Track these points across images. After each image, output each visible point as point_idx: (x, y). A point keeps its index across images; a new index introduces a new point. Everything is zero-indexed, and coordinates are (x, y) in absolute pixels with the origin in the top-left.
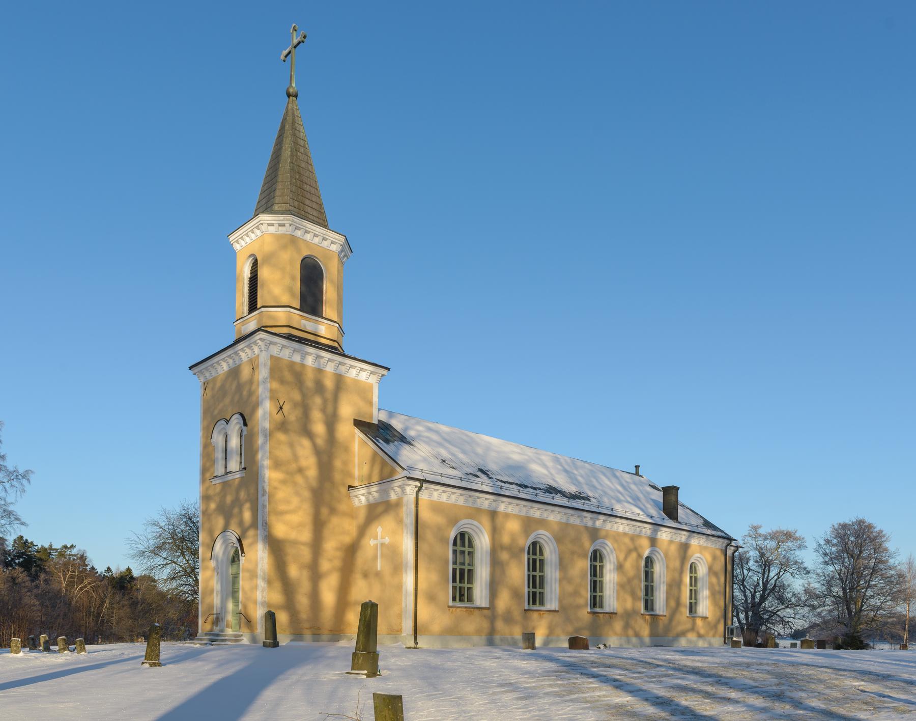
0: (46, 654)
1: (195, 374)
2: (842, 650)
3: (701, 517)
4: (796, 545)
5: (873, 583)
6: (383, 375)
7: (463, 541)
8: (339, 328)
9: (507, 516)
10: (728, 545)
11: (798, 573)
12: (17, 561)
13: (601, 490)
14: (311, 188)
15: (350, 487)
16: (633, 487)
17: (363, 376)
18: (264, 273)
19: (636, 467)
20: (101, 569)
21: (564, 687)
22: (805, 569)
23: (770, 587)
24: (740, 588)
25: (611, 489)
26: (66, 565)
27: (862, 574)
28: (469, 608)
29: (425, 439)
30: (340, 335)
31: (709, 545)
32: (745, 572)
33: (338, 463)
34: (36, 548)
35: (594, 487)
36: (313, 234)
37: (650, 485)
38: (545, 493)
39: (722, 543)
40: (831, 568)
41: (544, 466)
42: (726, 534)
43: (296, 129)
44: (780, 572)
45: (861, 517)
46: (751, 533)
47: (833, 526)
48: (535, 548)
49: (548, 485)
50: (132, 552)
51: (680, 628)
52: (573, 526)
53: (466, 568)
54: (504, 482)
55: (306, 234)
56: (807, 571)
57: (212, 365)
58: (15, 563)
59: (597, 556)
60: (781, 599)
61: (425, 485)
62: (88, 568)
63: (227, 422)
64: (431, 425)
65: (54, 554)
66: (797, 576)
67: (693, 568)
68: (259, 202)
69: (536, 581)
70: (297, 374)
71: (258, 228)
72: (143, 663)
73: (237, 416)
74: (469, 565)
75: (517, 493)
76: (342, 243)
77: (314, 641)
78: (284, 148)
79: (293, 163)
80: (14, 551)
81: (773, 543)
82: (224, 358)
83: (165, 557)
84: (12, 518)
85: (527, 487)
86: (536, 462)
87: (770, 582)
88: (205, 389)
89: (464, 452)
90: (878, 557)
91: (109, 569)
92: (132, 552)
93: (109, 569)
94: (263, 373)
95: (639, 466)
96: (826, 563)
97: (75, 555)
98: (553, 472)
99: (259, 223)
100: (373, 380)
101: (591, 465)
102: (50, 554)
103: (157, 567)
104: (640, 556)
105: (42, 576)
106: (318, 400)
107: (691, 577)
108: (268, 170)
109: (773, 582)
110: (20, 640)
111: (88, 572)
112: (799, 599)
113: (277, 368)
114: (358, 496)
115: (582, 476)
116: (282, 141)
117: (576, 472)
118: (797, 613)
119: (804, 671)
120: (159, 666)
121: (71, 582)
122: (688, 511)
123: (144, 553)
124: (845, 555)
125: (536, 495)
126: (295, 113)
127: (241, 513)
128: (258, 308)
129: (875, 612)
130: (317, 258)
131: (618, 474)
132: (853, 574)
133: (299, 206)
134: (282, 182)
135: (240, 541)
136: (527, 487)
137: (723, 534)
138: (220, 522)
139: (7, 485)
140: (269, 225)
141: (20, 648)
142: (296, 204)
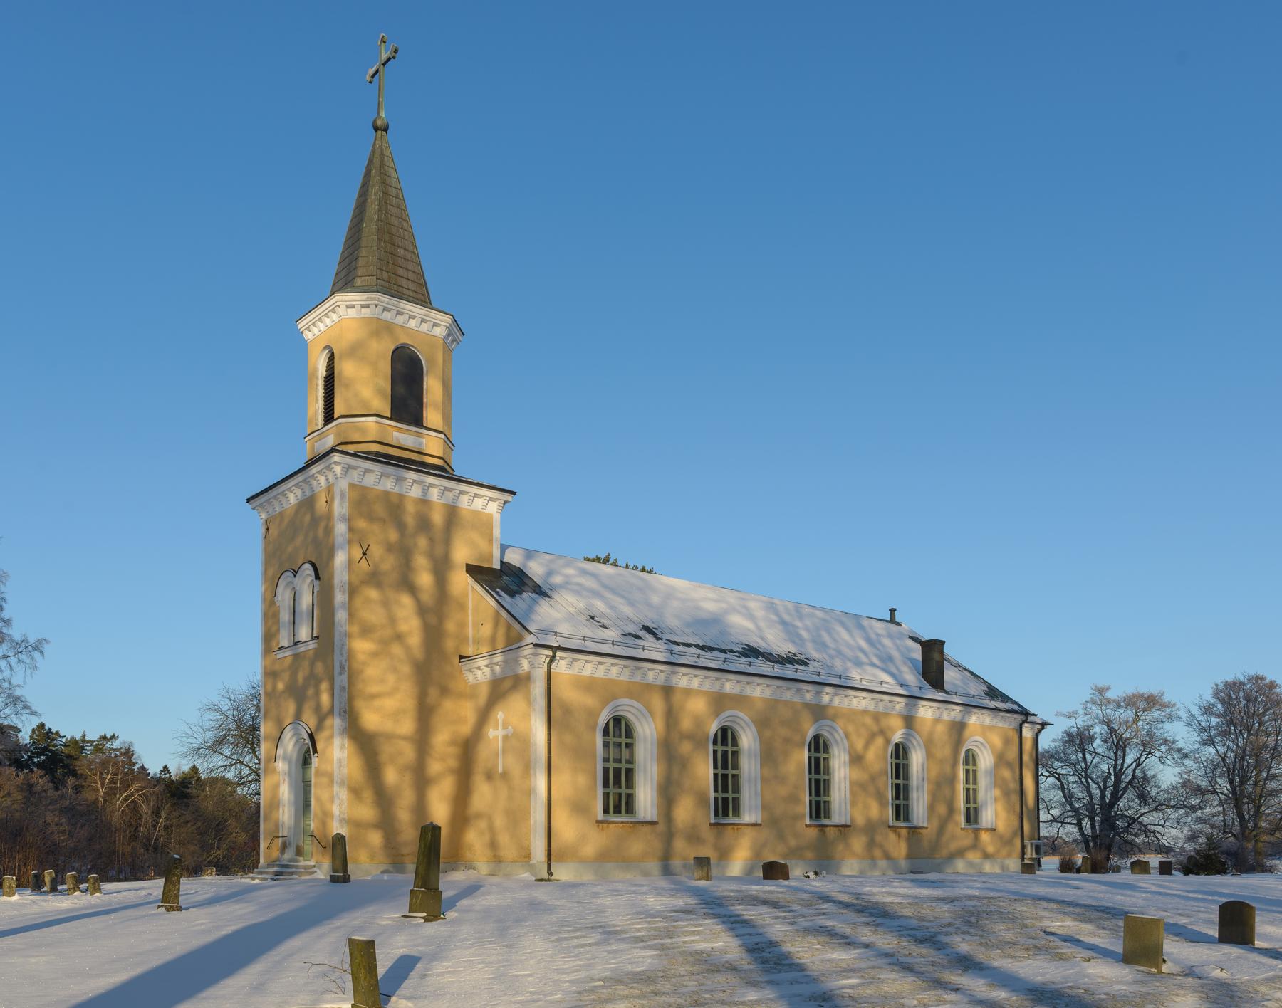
0: (50, 897)
1: (254, 508)
2: (1191, 875)
3: (985, 681)
4: (1164, 714)
6: (506, 502)
7: (619, 730)
8: (446, 439)
9: (688, 692)
11: (1170, 757)
12: (36, 760)
14: (406, 253)
15: (461, 657)
16: (886, 642)
17: (478, 504)
18: (346, 369)
19: (891, 610)
20: (154, 769)
22: (1179, 750)
23: (1127, 778)
24: (1082, 782)
25: (849, 646)
26: (104, 764)
28: (627, 822)
29: (576, 588)
30: (448, 449)
31: (1000, 724)
32: (1088, 757)
33: (450, 626)
34: (64, 740)
35: (824, 645)
36: (408, 315)
37: (910, 637)
38: (739, 657)
39: (1007, 724)
41: (751, 617)
43: (385, 175)
47: (1217, 685)
48: (726, 736)
49: (746, 645)
51: (953, 846)
53: (624, 766)
54: (678, 644)
57: (275, 497)
58: (33, 763)
59: (819, 746)
60: (1143, 797)
61: (559, 654)
62: (136, 768)
63: (295, 573)
65: (88, 748)
66: (1168, 762)
67: (970, 758)
68: (337, 274)
69: (727, 781)
70: (394, 506)
71: (334, 311)
72: (159, 907)
73: (307, 566)
76: (448, 325)
78: (369, 201)
79: (381, 221)
80: (32, 745)
81: (1129, 712)
82: (290, 488)
83: (228, 754)
84: (20, 706)
86: (739, 612)
88: (268, 529)
89: (631, 603)
91: (166, 769)
92: (181, 749)
93: (166, 769)
94: (340, 508)
95: (895, 610)
97: (117, 750)
98: (762, 624)
99: (334, 306)
100: (493, 509)
101: (824, 611)
102: (83, 748)
103: (217, 769)
104: (888, 741)
105: (71, 781)
106: (422, 542)
107: (967, 771)
108: (349, 231)
109: (1130, 771)
110: (14, 878)
111: (135, 774)
113: (362, 501)
115: (807, 629)
116: (367, 190)
117: (799, 624)
118: (1168, 819)
120: (178, 910)
121: (111, 789)
122: (967, 673)
123: (199, 749)
125: (724, 661)
127: (317, 693)
128: (335, 417)
130: (414, 347)
131: (865, 623)
133: (389, 278)
134: (367, 247)
135: (311, 736)
136: (712, 649)
137: (1015, 707)
138: (291, 707)
139: (13, 660)
140: (348, 307)
141: (15, 889)
142: (385, 275)
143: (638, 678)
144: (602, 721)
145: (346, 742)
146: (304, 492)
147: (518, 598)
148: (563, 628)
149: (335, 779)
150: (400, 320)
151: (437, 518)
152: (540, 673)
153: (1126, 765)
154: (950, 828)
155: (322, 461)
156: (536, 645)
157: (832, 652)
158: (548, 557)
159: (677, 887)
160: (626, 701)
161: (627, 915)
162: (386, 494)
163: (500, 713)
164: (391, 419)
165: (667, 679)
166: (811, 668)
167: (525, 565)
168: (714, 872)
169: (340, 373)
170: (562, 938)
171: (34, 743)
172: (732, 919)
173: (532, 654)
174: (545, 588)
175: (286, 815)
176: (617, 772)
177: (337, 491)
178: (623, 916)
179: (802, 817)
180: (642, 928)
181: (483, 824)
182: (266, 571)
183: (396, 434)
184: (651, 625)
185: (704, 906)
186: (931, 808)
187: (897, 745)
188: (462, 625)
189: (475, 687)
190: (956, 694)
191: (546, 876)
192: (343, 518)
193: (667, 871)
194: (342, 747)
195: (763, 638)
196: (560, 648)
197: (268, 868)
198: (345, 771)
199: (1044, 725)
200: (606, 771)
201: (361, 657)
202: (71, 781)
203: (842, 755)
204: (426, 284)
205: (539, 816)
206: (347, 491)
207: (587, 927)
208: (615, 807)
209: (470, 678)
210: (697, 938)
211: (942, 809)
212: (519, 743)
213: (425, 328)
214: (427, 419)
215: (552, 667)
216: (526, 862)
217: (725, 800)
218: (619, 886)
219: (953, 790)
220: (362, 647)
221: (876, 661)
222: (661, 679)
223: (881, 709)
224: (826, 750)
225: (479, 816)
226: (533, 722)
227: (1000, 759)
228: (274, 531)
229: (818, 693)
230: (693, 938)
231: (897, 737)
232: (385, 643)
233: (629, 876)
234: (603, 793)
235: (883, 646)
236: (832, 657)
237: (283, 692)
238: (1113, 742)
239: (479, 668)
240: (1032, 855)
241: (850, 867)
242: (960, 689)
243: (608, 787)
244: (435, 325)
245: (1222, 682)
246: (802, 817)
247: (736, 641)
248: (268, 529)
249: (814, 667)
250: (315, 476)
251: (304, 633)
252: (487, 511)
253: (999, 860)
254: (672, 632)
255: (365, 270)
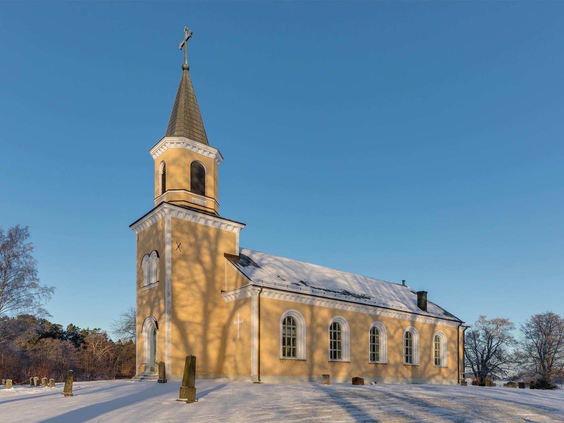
1: (132, 230)
4: (508, 327)
5: (559, 350)
6: (241, 228)
7: (290, 322)
9: (320, 308)
10: (460, 325)
11: (510, 343)
13: (381, 294)
14: (197, 122)
15: (222, 291)
16: (402, 292)
17: (229, 229)
18: (171, 170)
19: (403, 281)
21: (306, 411)
22: (515, 341)
23: (492, 351)
24: (474, 351)
25: (387, 293)
26: (96, 339)
27: (551, 344)
28: (293, 360)
30: (217, 206)
31: (450, 326)
32: (477, 342)
33: (218, 278)
37: (411, 291)
39: (454, 325)
40: (531, 341)
41: (346, 280)
42: (458, 319)
43: (188, 88)
44: (499, 342)
45: (550, 311)
46: (480, 320)
48: (335, 326)
49: (344, 290)
50: (113, 330)
51: (431, 373)
52: (362, 314)
53: (292, 337)
54: (316, 288)
55: (193, 148)
56: (516, 342)
59: (374, 331)
60: (500, 358)
61: (264, 289)
62: (108, 340)
63: (149, 255)
64: (276, 257)
65: (90, 333)
66: (510, 345)
67: (437, 339)
70: (193, 228)
71: (165, 145)
73: (154, 252)
74: (293, 335)
75: (323, 294)
77: (473, 385)
78: (180, 99)
80: (68, 332)
81: (494, 326)
85: (330, 291)
87: (493, 348)
88: (138, 238)
89: (296, 272)
90: (562, 335)
94: (167, 227)
95: (405, 281)
96: (527, 337)
97: (100, 334)
98: (351, 283)
99: (165, 143)
100: (236, 231)
102: (88, 333)
104: (404, 330)
106: (205, 243)
107: (436, 344)
109: (494, 348)
112: (512, 358)
113: (178, 225)
114: (230, 295)
115: (369, 286)
117: (366, 284)
118: (510, 366)
119: (491, 403)
120: (71, 396)
122: (435, 306)
124: (540, 333)
125: (335, 296)
126: (187, 79)
127: (159, 304)
129: (561, 367)
130: (201, 162)
131: (393, 285)
132: (545, 344)
133: (190, 132)
135: (156, 323)
136: (330, 291)
137: (456, 319)
138: (149, 310)
139: (41, 295)
140: (171, 143)
142: (188, 131)
143: (298, 301)
144: (282, 318)
145: (171, 324)
146: (152, 221)
147: (246, 268)
148: (266, 280)
149: (166, 340)
150: (194, 150)
151: (212, 233)
152: (256, 297)
153: (492, 346)
154: (429, 366)
155: (159, 207)
156: (254, 285)
157: (380, 295)
158: (261, 253)
159: (316, 387)
160: (293, 310)
161: (292, 401)
162: (189, 223)
163: (238, 314)
164: (191, 192)
165: (311, 302)
166: (371, 300)
167: (251, 256)
168: (331, 381)
169: (168, 172)
170: (254, 415)
171: (68, 331)
172: (347, 405)
173: (252, 289)
174: (258, 264)
175: (147, 355)
176: (289, 339)
177: (166, 220)
178: (289, 402)
179: (368, 360)
180: (299, 410)
181: (232, 359)
182: (138, 255)
183: (193, 198)
184: (304, 281)
185: (330, 397)
186: (421, 358)
187: (407, 333)
188: (223, 278)
189: (228, 303)
190: (432, 313)
191: (257, 381)
192: (169, 231)
193: (311, 380)
194: (169, 326)
195: (352, 288)
196: (264, 287)
197: (139, 376)
198: (170, 336)
199: (467, 327)
200: (284, 339)
201: (178, 290)
202: (82, 345)
203: (384, 335)
204: (205, 132)
205: (255, 356)
206: (170, 220)
207: (269, 408)
208: (288, 354)
209: (226, 300)
210: (330, 416)
211: (426, 359)
212: (247, 326)
213: (206, 154)
214: (207, 193)
215: (261, 295)
216: (249, 375)
217: (335, 352)
218: (289, 386)
219: (431, 351)
220: (178, 285)
221: (398, 299)
222: (308, 302)
223: (401, 317)
224: (378, 333)
225: (230, 356)
226: (252, 317)
227: (450, 340)
228: (141, 238)
229: (375, 310)
230: (327, 417)
231: (408, 329)
232: (189, 284)
233: (294, 382)
234: (283, 348)
235: (401, 294)
236: (380, 297)
237: (145, 304)
238: (487, 337)
239: (229, 296)
240: (461, 378)
241: (388, 380)
242: (434, 311)
243: (285, 345)
244: (210, 153)
245: (535, 315)
246: (368, 360)
247: (340, 289)
248: (138, 238)
249: (373, 300)
250: (157, 214)
251: (153, 280)
252: (233, 231)
253: (449, 380)
254: (313, 284)
255: (179, 128)
